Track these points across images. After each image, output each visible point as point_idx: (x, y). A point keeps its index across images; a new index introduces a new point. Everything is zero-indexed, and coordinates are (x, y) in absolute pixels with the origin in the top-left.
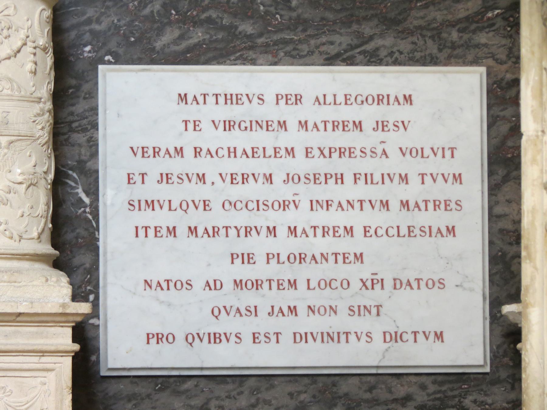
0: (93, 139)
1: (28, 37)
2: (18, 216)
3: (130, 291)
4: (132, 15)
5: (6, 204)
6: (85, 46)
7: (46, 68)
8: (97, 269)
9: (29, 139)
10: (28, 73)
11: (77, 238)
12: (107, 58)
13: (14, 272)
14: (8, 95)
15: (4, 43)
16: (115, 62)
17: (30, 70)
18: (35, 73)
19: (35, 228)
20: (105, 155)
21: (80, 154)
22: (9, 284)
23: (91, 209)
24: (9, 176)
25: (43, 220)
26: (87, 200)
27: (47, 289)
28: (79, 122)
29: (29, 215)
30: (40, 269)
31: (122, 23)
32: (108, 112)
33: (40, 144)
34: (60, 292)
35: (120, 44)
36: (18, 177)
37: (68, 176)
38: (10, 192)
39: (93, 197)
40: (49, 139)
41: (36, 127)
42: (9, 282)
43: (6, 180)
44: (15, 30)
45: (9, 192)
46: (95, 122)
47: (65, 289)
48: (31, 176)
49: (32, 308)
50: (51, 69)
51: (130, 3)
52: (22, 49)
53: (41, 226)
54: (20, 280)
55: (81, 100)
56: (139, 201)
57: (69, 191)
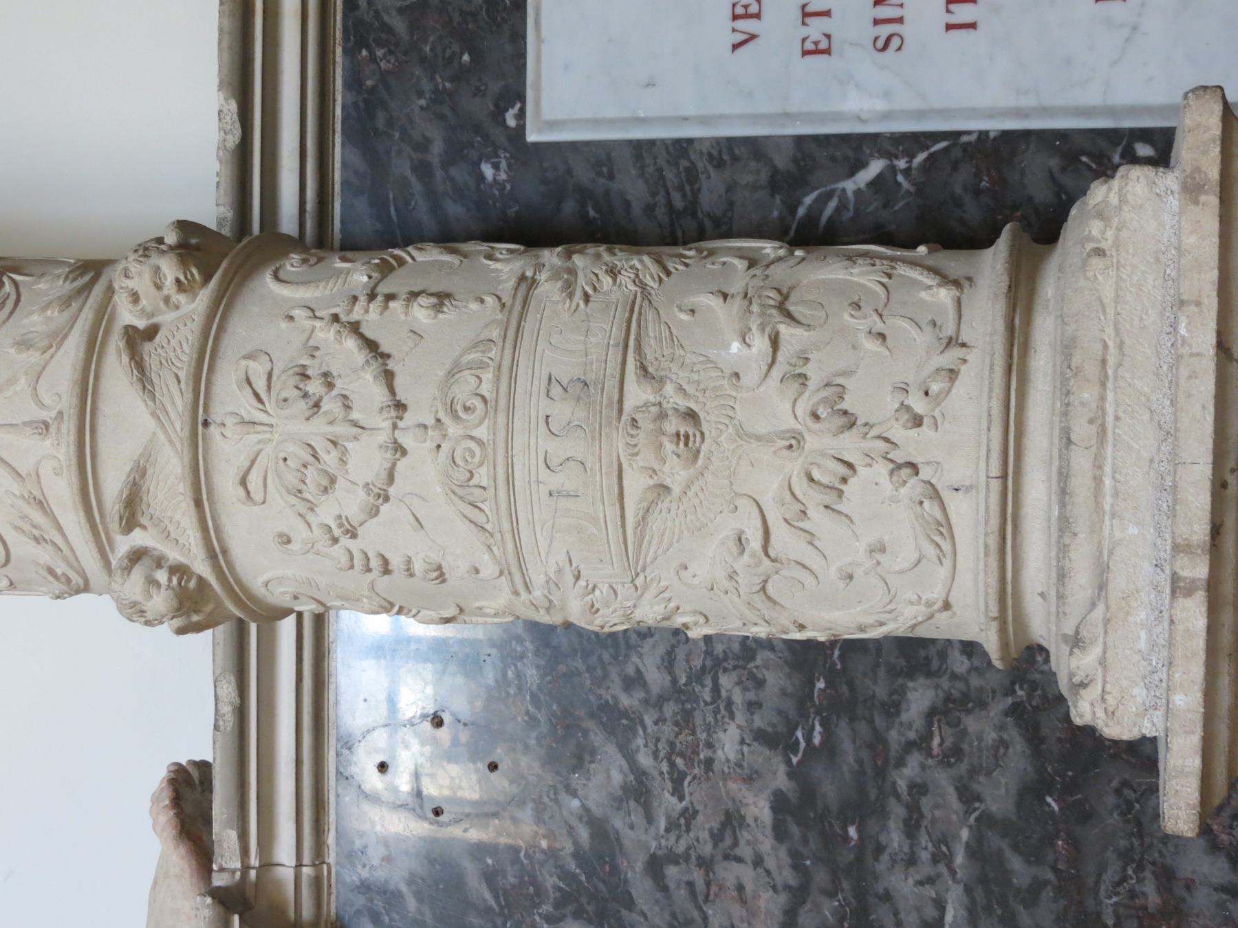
0: (715, 153)
1: (335, 318)
2: (882, 350)
3: (1127, 40)
4: (407, 62)
5: (839, 389)
6: (482, 177)
7: (450, 265)
8: (1063, 135)
9: (640, 314)
10: (441, 316)
11: (977, 192)
12: (511, 122)
13: (1069, 367)
14: (497, 379)
15: (344, 393)
16: (521, 102)
17: (431, 312)
18: (442, 298)
19: (924, 295)
20: (755, 118)
21: (755, 187)
22: (1110, 385)
23: (900, 154)
24: (750, 379)
25: (903, 270)
26: (875, 167)
27: (1131, 251)
28: (671, 190)
29: (881, 316)
30: (1059, 278)
31: (426, 85)
32: (640, 112)
33: (661, 280)
34: (1141, 207)
35: (477, 89)
36: (754, 350)
37: (812, 218)
38: (805, 376)
39: (868, 152)
40: (649, 254)
41: (608, 293)
42: (1103, 385)
43: (762, 389)
44: (313, 356)
45: (801, 381)
46: (671, 149)
47: (1129, 188)
48: (755, 308)
49: (1198, 304)
50: (453, 251)
51: (380, 67)
52: (369, 334)
53: (920, 278)
54: (1098, 347)
55: (615, 186)
56: (877, 22)
57: (851, 214)
